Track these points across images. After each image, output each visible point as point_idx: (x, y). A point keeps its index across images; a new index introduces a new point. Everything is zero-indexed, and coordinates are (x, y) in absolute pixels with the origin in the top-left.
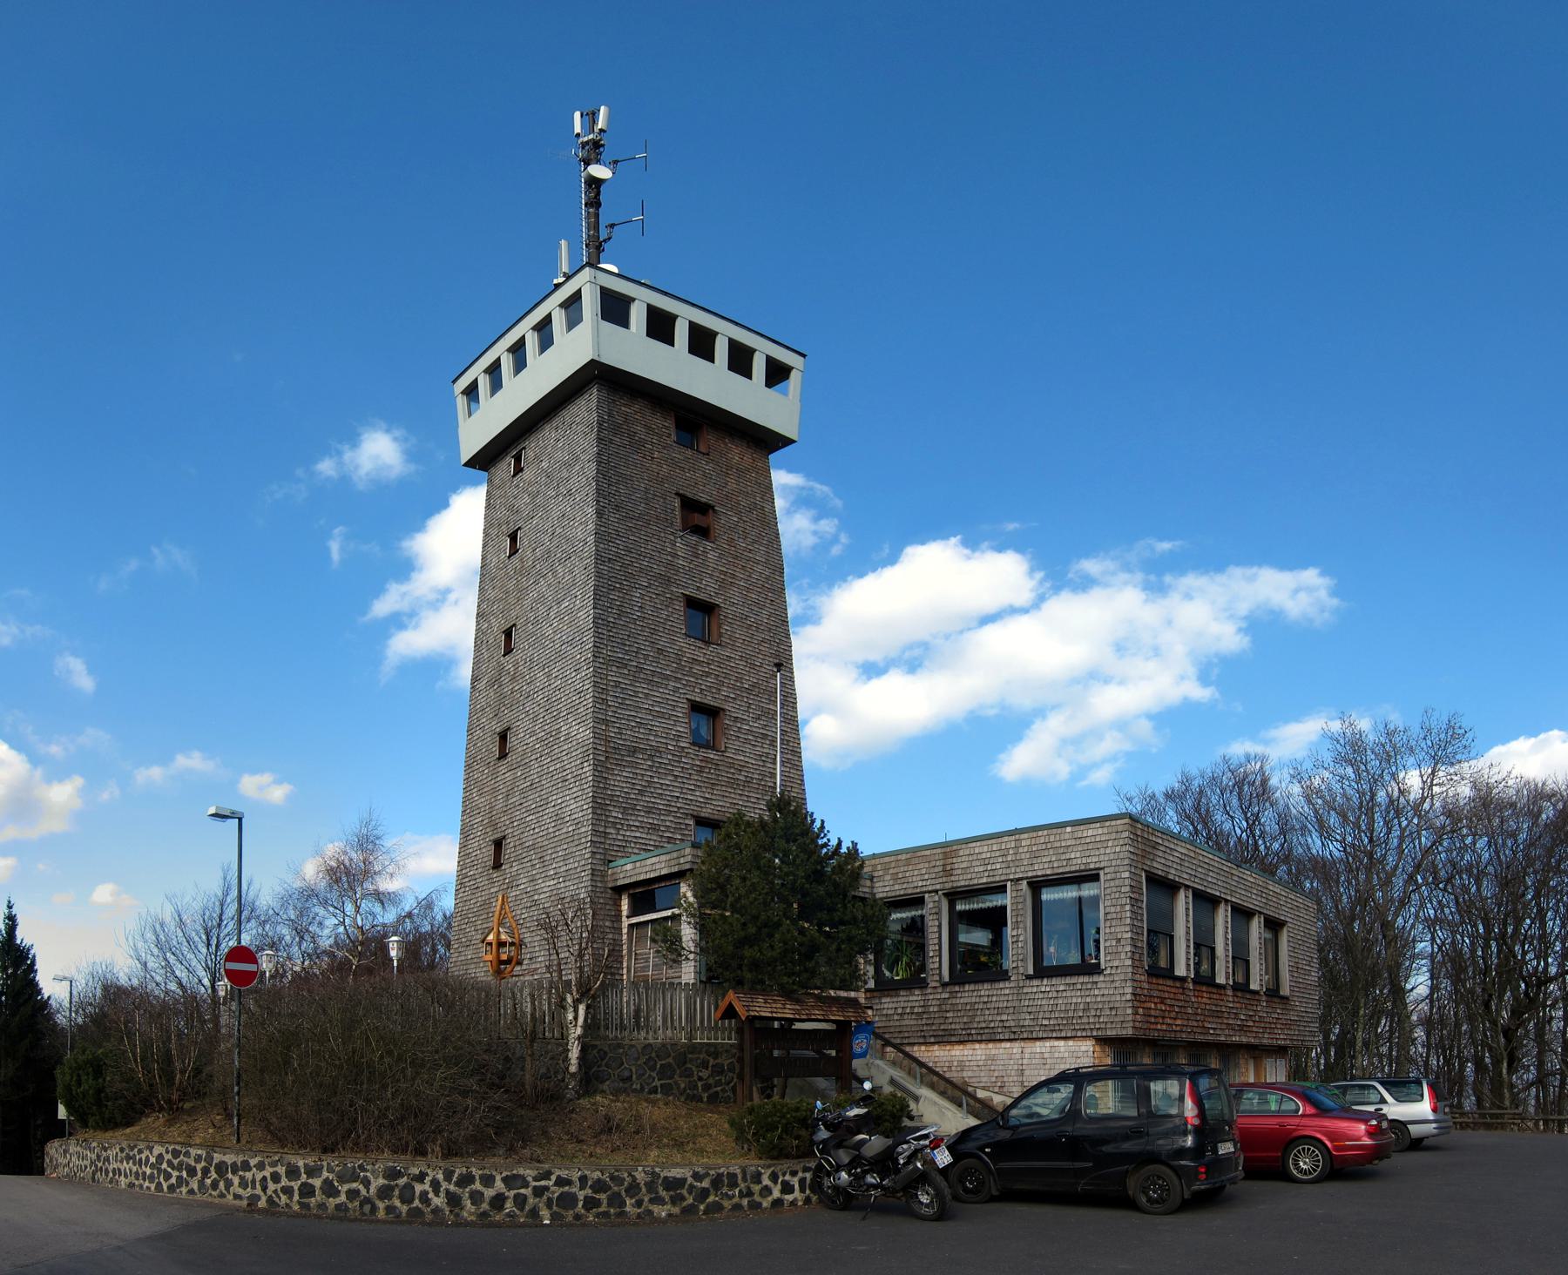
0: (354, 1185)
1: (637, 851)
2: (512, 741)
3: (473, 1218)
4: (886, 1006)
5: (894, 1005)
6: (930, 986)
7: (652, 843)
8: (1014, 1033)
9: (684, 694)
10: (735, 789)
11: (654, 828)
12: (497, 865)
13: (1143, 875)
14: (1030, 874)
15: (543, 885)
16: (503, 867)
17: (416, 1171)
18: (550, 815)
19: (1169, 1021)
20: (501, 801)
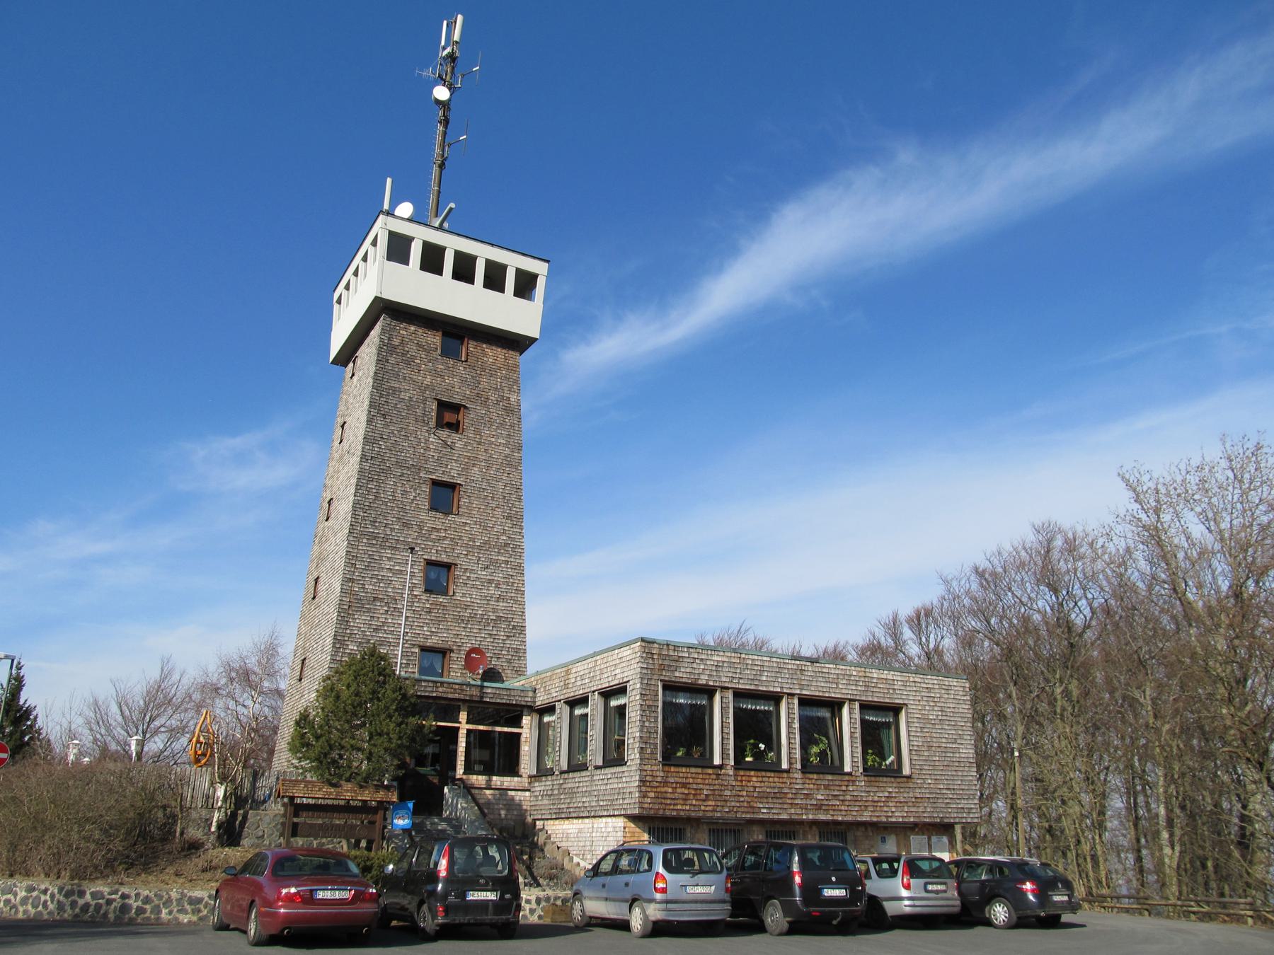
0: (9, 896)
3: (70, 918)
13: (660, 684)
14: (600, 687)
17: (43, 887)
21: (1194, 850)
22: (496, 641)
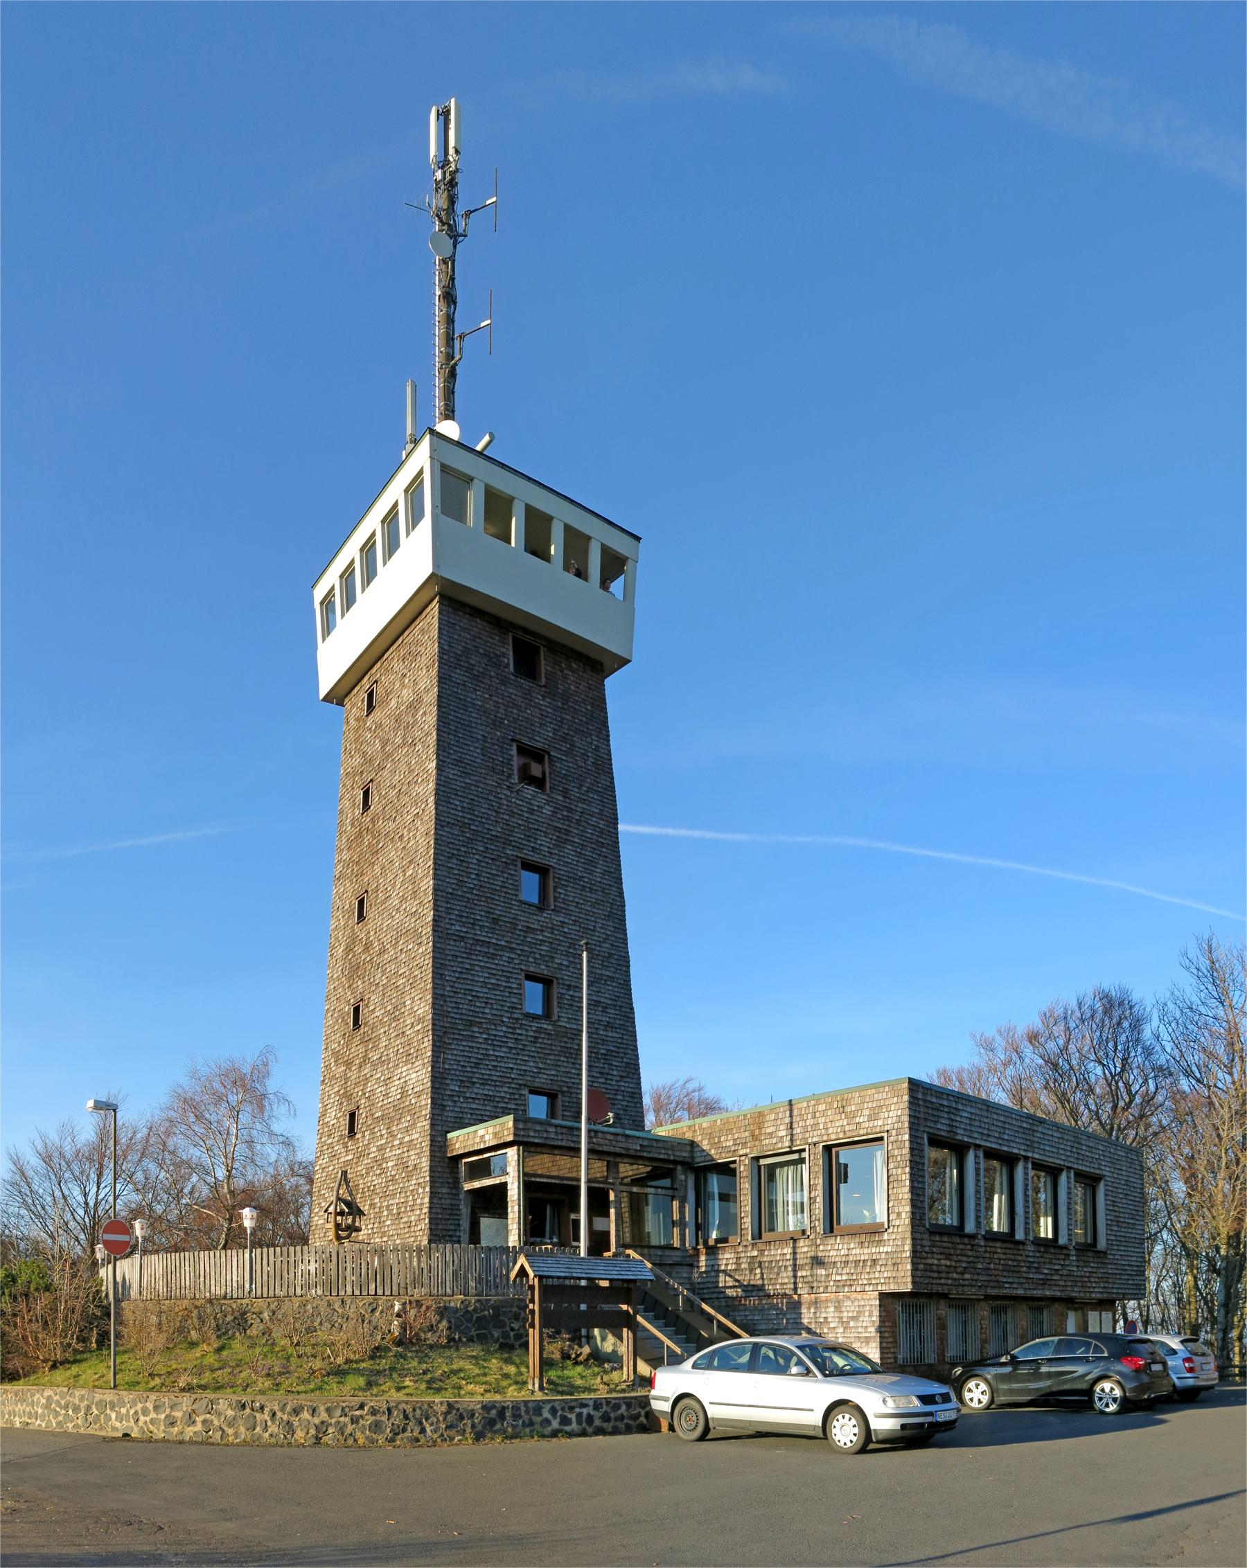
2: (364, 1012)
11: (489, 1099)
19: (955, 1276)
22: (609, 1082)
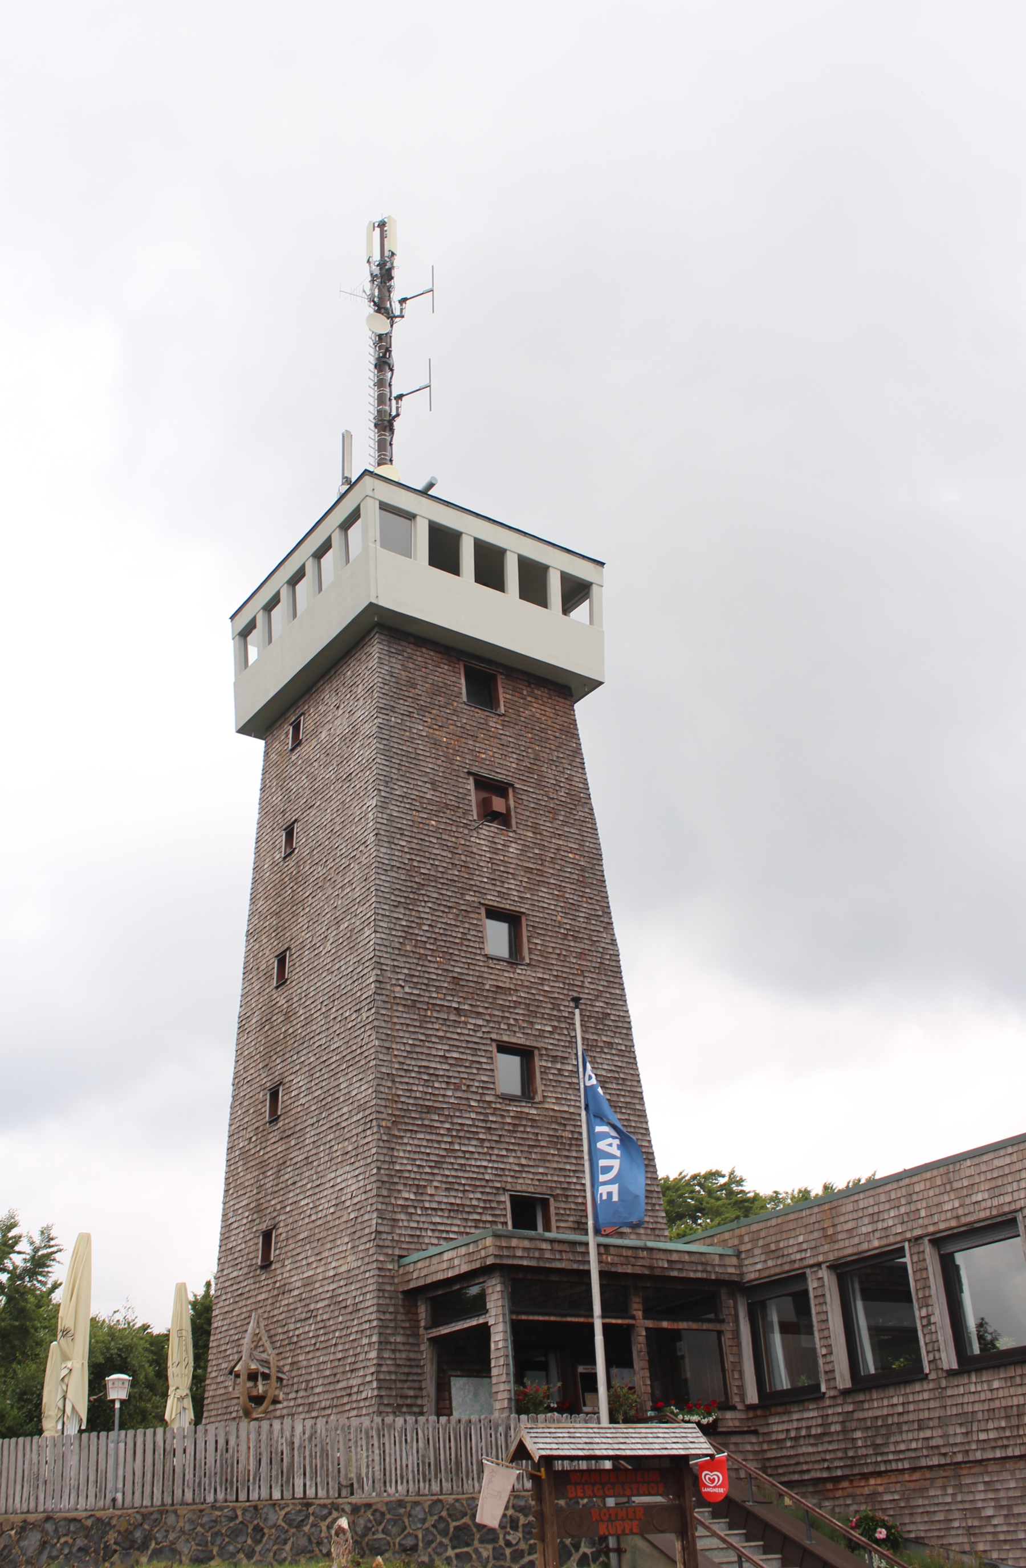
1: (435, 1241)
4: (775, 1428)
5: (785, 1426)
6: (827, 1396)
7: (455, 1229)
8: (945, 1454)
9: (488, 1032)
10: (559, 1149)
12: (266, 1264)
14: (931, 1229)
15: (320, 1290)
16: (273, 1267)
18: (328, 1198)
20: (271, 1178)
21: (289, 1539)
